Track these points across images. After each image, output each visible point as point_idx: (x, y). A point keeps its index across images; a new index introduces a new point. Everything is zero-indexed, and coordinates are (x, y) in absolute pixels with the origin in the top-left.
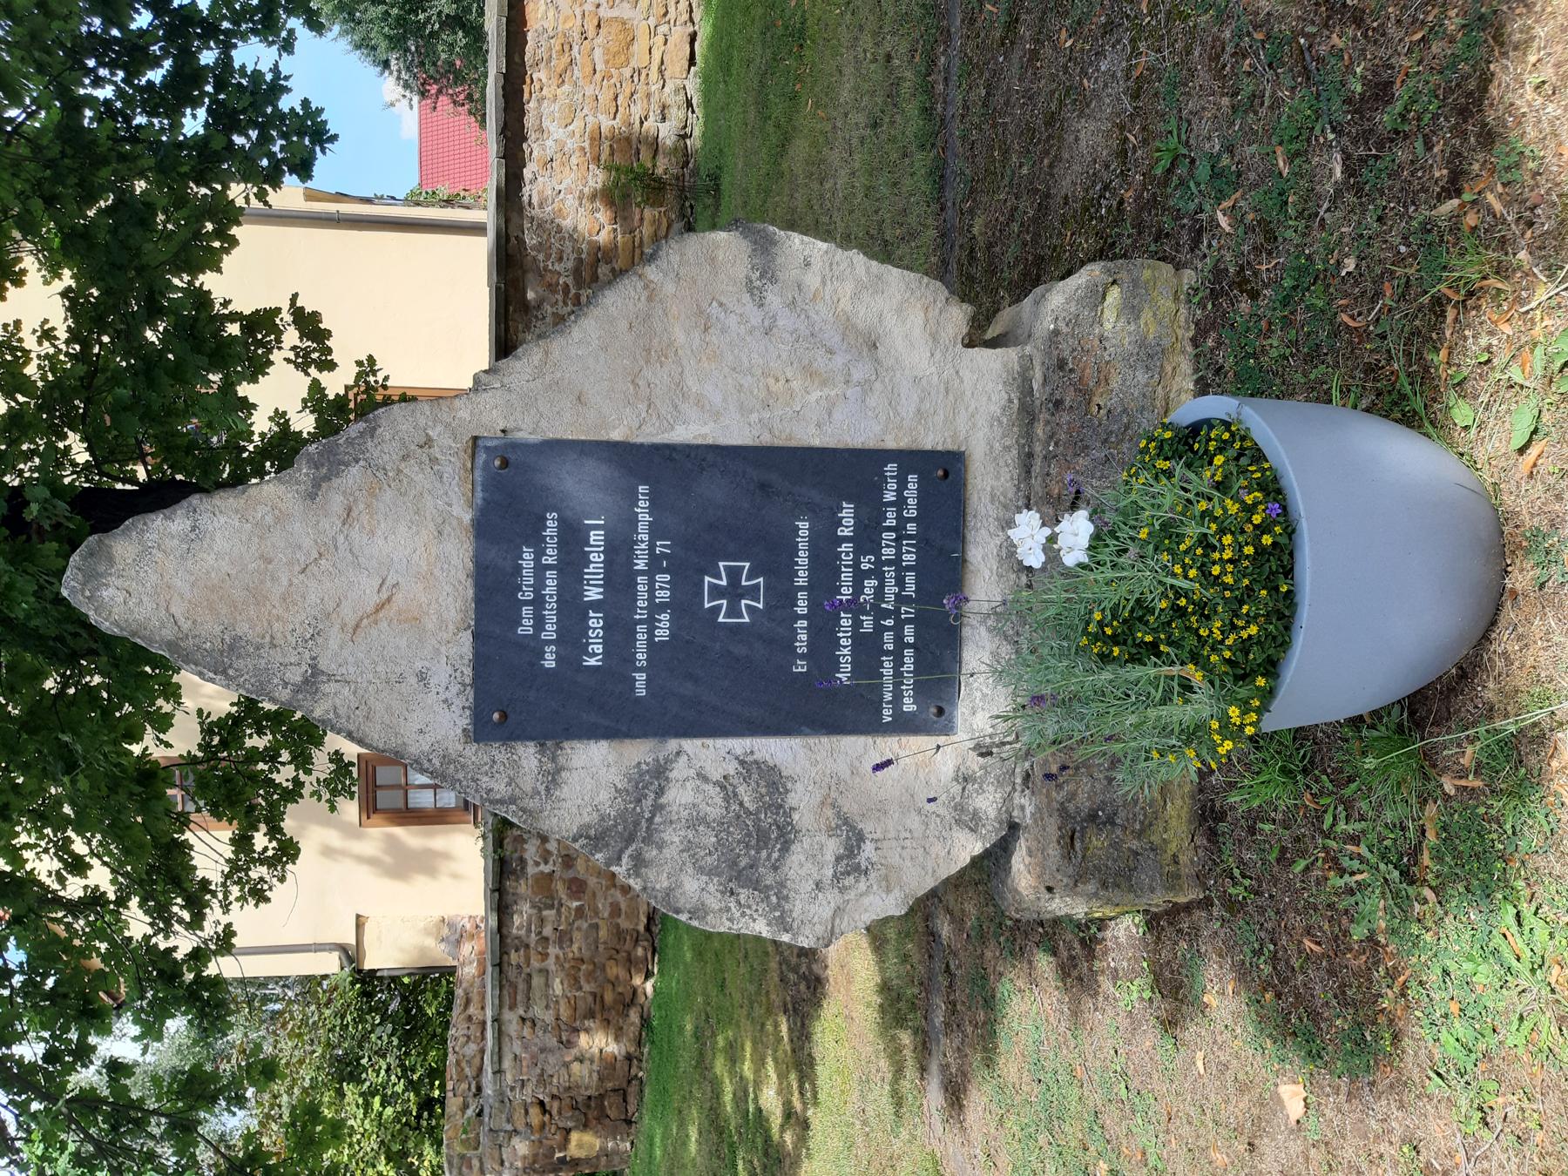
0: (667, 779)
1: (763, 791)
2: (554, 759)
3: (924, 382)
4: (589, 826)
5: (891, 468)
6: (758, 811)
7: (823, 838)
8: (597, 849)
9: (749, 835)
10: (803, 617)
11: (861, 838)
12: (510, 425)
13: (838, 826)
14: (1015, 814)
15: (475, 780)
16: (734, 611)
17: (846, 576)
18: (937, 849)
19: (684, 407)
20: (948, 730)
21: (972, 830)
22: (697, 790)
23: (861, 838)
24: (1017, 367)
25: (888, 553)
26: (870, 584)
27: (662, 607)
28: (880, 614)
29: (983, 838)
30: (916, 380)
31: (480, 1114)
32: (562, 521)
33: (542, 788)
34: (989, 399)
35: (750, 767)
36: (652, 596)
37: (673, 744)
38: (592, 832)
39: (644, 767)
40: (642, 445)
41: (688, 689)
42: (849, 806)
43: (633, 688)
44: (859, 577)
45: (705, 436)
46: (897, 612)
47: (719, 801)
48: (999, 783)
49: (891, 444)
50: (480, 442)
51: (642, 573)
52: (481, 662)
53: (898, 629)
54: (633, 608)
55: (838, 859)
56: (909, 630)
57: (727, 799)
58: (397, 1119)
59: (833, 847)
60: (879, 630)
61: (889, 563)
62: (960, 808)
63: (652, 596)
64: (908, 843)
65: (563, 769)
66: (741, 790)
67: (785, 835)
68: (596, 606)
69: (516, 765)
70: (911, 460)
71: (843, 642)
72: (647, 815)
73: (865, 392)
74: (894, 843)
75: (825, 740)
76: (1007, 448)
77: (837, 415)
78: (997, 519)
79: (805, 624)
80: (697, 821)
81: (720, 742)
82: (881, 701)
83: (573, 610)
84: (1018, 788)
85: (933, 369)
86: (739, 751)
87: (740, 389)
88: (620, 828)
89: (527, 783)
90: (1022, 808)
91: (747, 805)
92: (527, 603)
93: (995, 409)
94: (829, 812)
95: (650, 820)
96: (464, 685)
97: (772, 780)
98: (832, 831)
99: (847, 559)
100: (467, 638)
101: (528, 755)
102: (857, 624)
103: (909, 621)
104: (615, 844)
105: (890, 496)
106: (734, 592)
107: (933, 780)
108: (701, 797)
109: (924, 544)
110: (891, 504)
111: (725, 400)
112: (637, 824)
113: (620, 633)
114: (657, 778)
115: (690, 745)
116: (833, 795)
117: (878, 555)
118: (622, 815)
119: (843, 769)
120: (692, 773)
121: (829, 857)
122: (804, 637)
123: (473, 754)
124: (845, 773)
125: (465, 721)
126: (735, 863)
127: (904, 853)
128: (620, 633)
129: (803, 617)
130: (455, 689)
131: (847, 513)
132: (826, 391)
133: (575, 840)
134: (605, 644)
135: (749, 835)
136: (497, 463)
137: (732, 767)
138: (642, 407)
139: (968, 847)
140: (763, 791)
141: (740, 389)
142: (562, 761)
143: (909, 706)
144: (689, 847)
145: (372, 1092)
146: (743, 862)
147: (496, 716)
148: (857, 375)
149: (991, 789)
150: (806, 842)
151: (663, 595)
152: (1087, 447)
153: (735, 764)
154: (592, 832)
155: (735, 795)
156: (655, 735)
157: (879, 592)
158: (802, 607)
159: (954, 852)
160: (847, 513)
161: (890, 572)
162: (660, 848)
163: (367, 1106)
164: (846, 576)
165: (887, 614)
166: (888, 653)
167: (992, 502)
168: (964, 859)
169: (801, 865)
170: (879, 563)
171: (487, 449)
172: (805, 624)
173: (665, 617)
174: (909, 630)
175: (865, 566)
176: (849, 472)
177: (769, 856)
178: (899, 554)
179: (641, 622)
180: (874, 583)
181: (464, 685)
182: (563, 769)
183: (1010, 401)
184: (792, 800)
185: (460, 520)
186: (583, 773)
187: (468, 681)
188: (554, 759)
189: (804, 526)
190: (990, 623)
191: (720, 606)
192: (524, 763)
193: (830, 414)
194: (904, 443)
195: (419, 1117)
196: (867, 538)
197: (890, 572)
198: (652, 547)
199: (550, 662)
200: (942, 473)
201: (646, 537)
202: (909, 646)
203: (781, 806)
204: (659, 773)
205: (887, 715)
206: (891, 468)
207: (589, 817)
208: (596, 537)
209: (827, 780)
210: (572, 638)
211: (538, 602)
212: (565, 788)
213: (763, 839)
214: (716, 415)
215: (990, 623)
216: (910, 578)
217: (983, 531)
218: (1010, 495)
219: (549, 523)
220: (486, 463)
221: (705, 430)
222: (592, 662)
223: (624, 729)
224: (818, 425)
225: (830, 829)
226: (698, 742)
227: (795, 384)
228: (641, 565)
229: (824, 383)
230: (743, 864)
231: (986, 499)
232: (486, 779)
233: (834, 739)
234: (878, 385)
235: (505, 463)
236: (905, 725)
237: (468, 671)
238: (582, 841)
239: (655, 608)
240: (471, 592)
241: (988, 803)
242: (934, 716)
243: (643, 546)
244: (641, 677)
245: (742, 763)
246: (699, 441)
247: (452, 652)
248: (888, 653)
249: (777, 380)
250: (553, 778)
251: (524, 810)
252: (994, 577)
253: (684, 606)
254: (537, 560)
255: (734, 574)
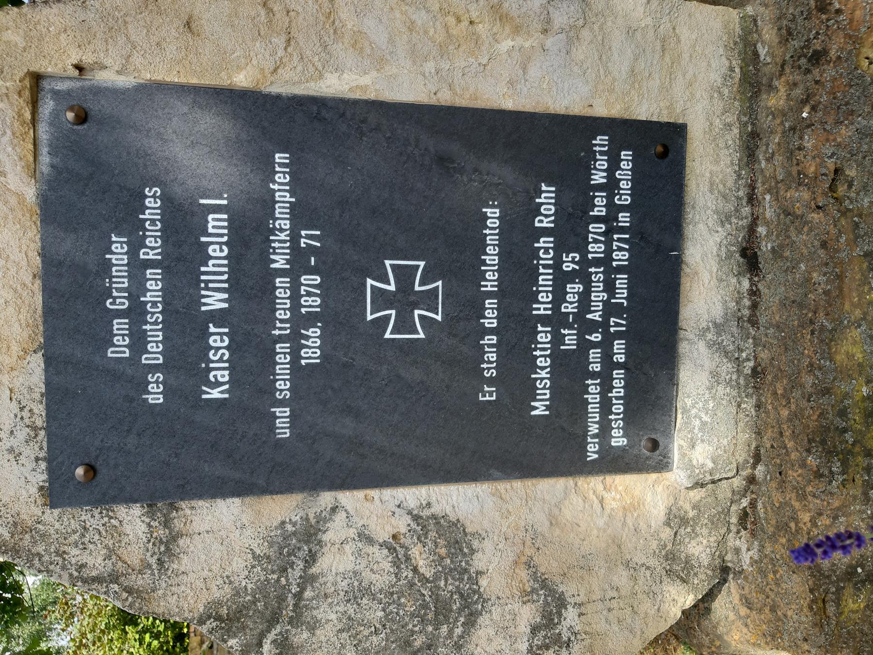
0: (320, 543)
1: (443, 551)
2: (167, 523)
3: (638, 35)
4: (219, 603)
5: (601, 141)
6: (436, 577)
7: (516, 606)
8: (230, 633)
9: (425, 606)
10: (491, 331)
11: (561, 603)
12: (88, 59)
13: (533, 591)
14: (728, 557)
15: (61, 554)
16: (404, 324)
17: (545, 279)
18: (646, 606)
19: (337, 49)
20: (662, 465)
21: (684, 581)
22: (359, 553)
23: (561, 603)
24: (738, 30)
25: (596, 249)
26: (574, 288)
27: (311, 319)
28: (585, 326)
29: (695, 589)
30: (631, 32)
31: (211, 647)
32: (167, 200)
33: (153, 561)
34: (709, 65)
35: (424, 523)
36: (296, 305)
37: (326, 498)
38: (224, 611)
39: (289, 528)
40: (278, 97)
41: (347, 426)
42: (548, 565)
43: (272, 428)
44: (561, 279)
45: (364, 88)
46: (605, 324)
47: (387, 565)
48: (714, 523)
49: (601, 110)
50: (46, 84)
51: (282, 273)
52: (55, 395)
53: (606, 346)
54: (271, 321)
55: (535, 630)
56: (619, 346)
57: (396, 564)
58: (161, 648)
59: (527, 615)
60: (584, 346)
61: (597, 262)
62: (671, 557)
63: (296, 305)
64: (614, 604)
65: (180, 535)
66: (416, 552)
67: (472, 607)
68: (219, 318)
69: (117, 532)
70: (626, 132)
71: (540, 362)
72: (294, 589)
73: (570, 42)
74: (600, 606)
75: (518, 484)
76: (728, 126)
77: (534, 72)
78: (716, 212)
79: (494, 339)
80: (358, 592)
81: (388, 493)
82: (585, 435)
83: (186, 324)
84: (734, 528)
85: (649, 21)
86: (412, 503)
87: (411, 27)
88: (260, 605)
89: (134, 554)
90: (737, 551)
91: (422, 570)
92: (119, 314)
93: (715, 77)
94: (523, 574)
95: (299, 596)
96: (35, 429)
97: (454, 539)
98: (527, 596)
99: (546, 258)
100: (37, 362)
101: (133, 520)
102: (557, 339)
103: (619, 335)
104: (254, 625)
105: (599, 178)
106: (405, 300)
107: (643, 526)
108: (364, 563)
109: (638, 238)
110: (600, 187)
111: (391, 41)
112: (281, 599)
113: (252, 355)
114: (307, 542)
115: (348, 499)
116: (529, 552)
117: (584, 252)
118: (262, 588)
119: (540, 519)
120: (352, 533)
121: (524, 628)
122: (493, 357)
123: (51, 516)
124: (543, 525)
125: (41, 477)
126: (408, 643)
127: (611, 616)
128: (252, 355)
129: (491, 331)
130: (22, 434)
131: (547, 197)
132: (519, 41)
133: (201, 622)
134: (232, 369)
135: (425, 606)
136: (70, 115)
137: (402, 523)
138: (279, 41)
139: (679, 599)
140: (443, 551)
141: (411, 27)
142: (178, 525)
143: (618, 440)
144: (349, 625)
145: (145, 631)
146: (419, 641)
147: (80, 471)
148: (560, 19)
149: (705, 531)
150: (496, 612)
151: (311, 303)
152: (852, 112)
153: (408, 519)
154: (224, 611)
155: (408, 558)
156: (302, 488)
157: (585, 299)
158: (490, 319)
159: (665, 607)
160: (547, 197)
161: (597, 274)
162: (312, 629)
163: (141, 641)
164: (545, 279)
165: (593, 326)
166: (594, 375)
167: (711, 191)
168: (675, 613)
169: (490, 640)
170: (585, 263)
171: (56, 94)
172: (494, 339)
173: (314, 332)
174: (619, 346)
175: (568, 267)
176: (551, 144)
177: (451, 632)
178: (609, 251)
179: (281, 339)
180: (579, 287)
181: (35, 429)
182: (180, 535)
183: (732, 69)
184: (479, 562)
185: (21, 198)
186: (209, 538)
187: (39, 423)
188: (167, 523)
189: (493, 214)
190: (709, 336)
191: (388, 317)
192: (127, 529)
193: (525, 70)
194: (615, 111)
195: (174, 647)
196: (570, 231)
197: (597, 274)
198: (295, 238)
199: (155, 395)
200: (660, 147)
201: (286, 224)
202: (619, 366)
203: (466, 571)
204: (310, 535)
205: (592, 450)
206: (601, 141)
207: (219, 592)
208: (216, 223)
209: (521, 534)
210: (186, 361)
211: (136, 312)
212: (185, 559)
213: (442, 612)
214: (380, 62)
215: (709, 336)
216: (621, 282)
217: (701, 226)
218: (730, 183)
219: (148, 202)
220: (56, 115)
221: (366, 80)
222: (215, 394)
223: (261, 482)
224: (511, 83)
225: (524, 593)
226: (360, 494)
227: (481, 29)
228: (280, 262)
229: (517, 30)
230: (418, 644)
231: (705, 188)
232: (75, 551)
233: (529, 482)
234: (585, 34)
235: (83, 118)
236: (614, 463)
237: (40, 409)
238: (211, 624)
239: (300, 320)
240: (39, 299)
241: (700, 548)
242: (649, 456)
243: (283, 236)
244: (282, 414)
245: (416, 518)
246: (357, 95)
247: (17, 383)
248: (594, 375)
249: (459, 20)
250: (167, 548)
251: (129, 591)
252: (714, 282)
253: (340, 317)
254: (133, 253)
255: (404, 276)
